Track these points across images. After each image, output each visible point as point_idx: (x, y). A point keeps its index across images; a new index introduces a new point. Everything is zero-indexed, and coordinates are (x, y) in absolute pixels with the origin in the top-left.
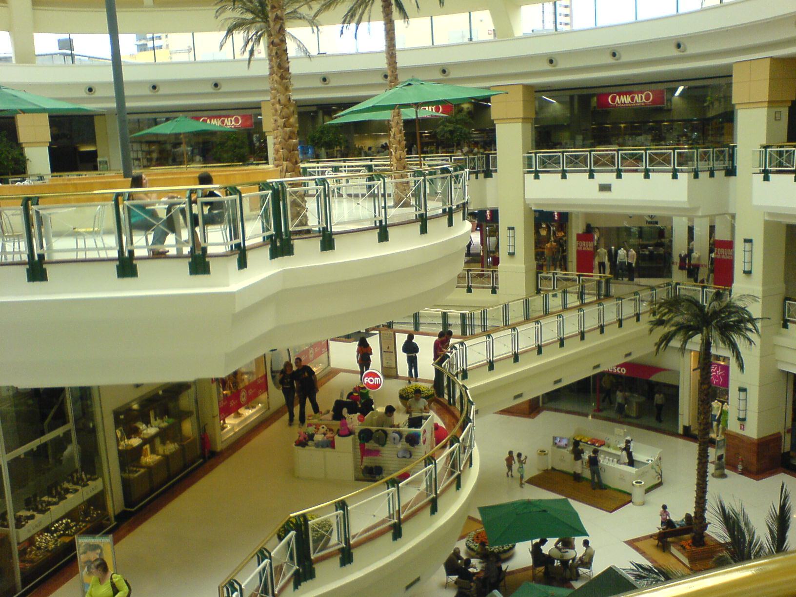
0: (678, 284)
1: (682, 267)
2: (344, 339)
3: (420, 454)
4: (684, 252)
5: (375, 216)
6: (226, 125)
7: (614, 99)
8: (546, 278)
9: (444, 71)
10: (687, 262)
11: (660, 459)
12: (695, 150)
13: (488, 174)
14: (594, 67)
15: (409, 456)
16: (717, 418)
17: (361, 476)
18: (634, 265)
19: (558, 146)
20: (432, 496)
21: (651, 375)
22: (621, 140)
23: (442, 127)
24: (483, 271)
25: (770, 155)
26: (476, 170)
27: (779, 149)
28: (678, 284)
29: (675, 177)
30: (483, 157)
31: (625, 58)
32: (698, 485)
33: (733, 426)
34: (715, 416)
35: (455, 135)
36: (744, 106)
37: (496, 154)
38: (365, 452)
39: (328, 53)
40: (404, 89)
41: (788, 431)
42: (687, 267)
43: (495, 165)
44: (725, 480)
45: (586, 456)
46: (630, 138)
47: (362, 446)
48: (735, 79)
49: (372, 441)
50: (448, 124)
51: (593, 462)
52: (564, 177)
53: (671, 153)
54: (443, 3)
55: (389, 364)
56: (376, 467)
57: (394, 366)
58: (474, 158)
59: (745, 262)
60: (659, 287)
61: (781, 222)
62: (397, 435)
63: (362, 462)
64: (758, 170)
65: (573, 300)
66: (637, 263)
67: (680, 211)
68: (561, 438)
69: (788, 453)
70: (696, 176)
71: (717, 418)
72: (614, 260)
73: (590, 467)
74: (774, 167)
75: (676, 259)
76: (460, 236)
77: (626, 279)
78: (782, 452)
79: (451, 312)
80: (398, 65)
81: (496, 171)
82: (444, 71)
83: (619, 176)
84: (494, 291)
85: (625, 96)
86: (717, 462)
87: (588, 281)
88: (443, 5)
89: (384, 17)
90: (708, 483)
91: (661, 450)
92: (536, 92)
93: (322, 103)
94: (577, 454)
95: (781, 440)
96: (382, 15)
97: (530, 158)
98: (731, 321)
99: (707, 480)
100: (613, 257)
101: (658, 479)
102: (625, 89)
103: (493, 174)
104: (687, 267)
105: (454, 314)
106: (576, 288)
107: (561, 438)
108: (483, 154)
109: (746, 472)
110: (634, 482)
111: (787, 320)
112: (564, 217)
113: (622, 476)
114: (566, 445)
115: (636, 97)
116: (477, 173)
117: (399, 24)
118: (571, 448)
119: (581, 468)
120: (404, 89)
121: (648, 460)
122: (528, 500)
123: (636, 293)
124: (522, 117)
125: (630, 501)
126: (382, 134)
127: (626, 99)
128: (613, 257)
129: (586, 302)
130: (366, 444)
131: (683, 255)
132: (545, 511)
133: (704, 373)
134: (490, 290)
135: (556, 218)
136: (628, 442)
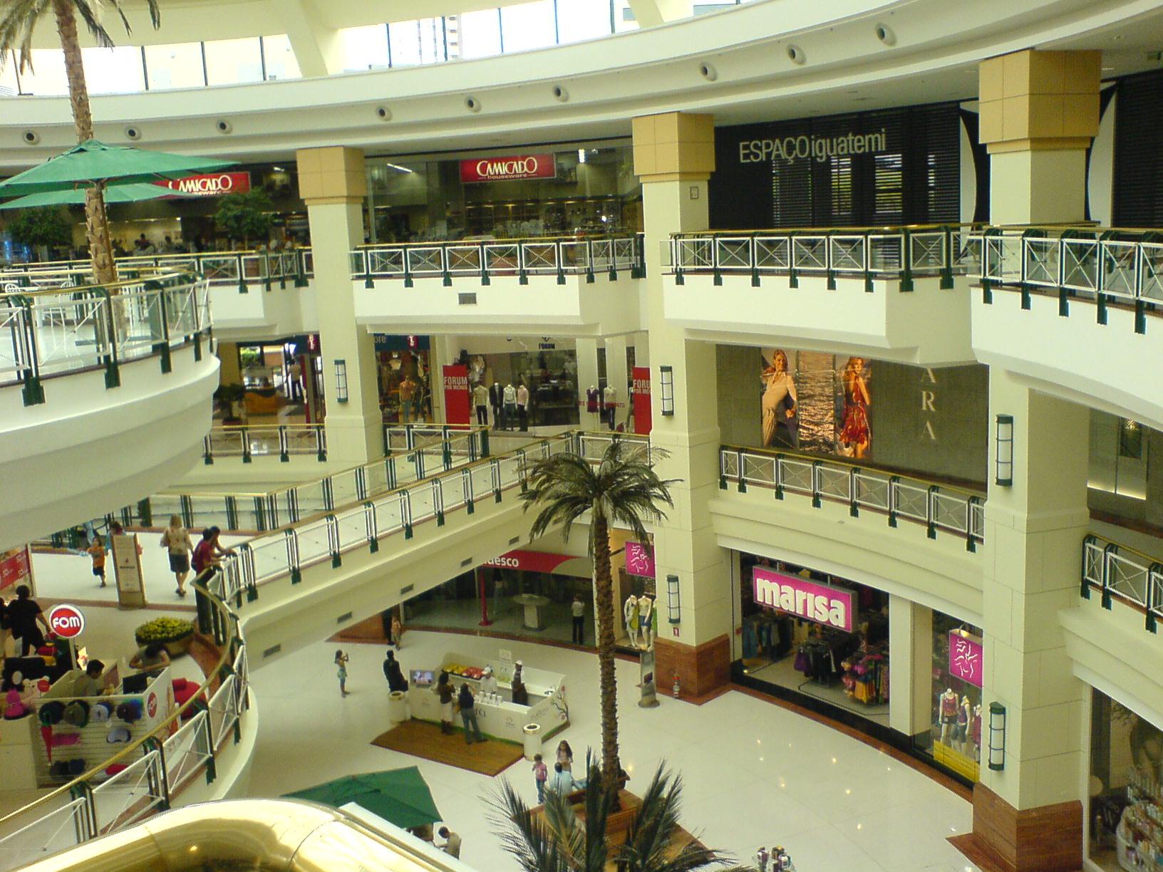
0: (581, 433)
1: (592, 409)
2: (51, 548)
3: (141, 733)
4: (594, 386)
5: (17, 365)
6: (209, 190)
7: (484, 168)
8: (398, 434)
9: (223, 126)
10: (598, 400)
11: (563, 689)
12: (587, 242)
13: (301, 282)
14: (498, 117)
15: (126, 738)
16: (646, 620)
17: (48, 778)
18: (526, 408)
19: (412, 238)
20: (158, 800)
21: (555, 566)
22: (500, 227)
23: (223, 210)
24: (309, 427)
25: (682, 247)
26: (281, 275)
27: (696, 240)
28: (581, 433)
29: (561, 281)
30: (290, 257)
31: (487, 108)
32: (604, 725)
33: (664, 631)
34: (644, 617)
35: (243, 222)
36: (315, 201)
37: (310, 250)
38: (51, 740)
39: (36, 94)
40: (72, 158)
41: (738, 632)
42: (598, 407)
43: (310, 267)
44: (656, 709)
45: (456, 696)
46: (514, 225)
47: (46, 733)
48: (636, 141)
49: (62, 721)
50: (232, 206)
51: (466, 701)
52: (409, 284)
53: (554, 246)
54: (159, 23)
55: (129, 587)
56: (73, 762)
57: (137, 588)
58: (278, 258)
59: (663, 399)
60: (557, 437)
61: (704, 341)
62: (103, 709)
63: (50, 756)
64: (669, 270)
65: (433, 464)
66: (530, 405)
67: (587, 329)
68: (423, 673)
69: (740, 661)
70: (591, 279)
71: (646, 620)
72: (498, 402)
73: (460, 709)
74: (690, 265)
75: (584, 398)
76: (187, 387)
77: (517, 429)
78: (732, 660)
79: (239, 495)
80: (93, 119)
81: (312, 276)
82: (223, 126)
83: (486, 282)
84: (322, 457)
85: (499, 164)
86: (644, 684)
87: (458, 435)
88: (159, 26)
89: (63, 41)
90: (618, 721)
91: (564, 676)
92: (367, 157)
93: (251, 162)
94: (445, 693)
95: (728, 644)
96: (58, 38)
97: (358, 257)
98: (632, 487)
99: (617, 716)
100: (496, 397)
101: (563, 718)
102: (499, 153)
103: (310, 281)
104: (598, 407)
105: (245, 498)
106: (439, 448)
107: (423, 673)
108: (292, 250)
109: (684, 695)
110: (525, 728)
111: (724, 476)
112: (423, 343)
113: (510, 720)
114: (430, 681)
115: (515, 165)
116: (283, 280)
117: (92, 55)
118: (436, 685)
119: (448, 713)
120: (72, 158)
121: (547, 693)
122: (353, 776)
123: (519, 451)
124: (346, 195)
125: (523, 756)
126: (152, 220)
127: (501, 169)
128: (496, 397)
129: (453, 467)
130: (53, 726)
131: (592, 392)
132: (377, 791)
133: (601, 565)
134: (317, 456)
135: (412, 344)
136: (519, 668)
